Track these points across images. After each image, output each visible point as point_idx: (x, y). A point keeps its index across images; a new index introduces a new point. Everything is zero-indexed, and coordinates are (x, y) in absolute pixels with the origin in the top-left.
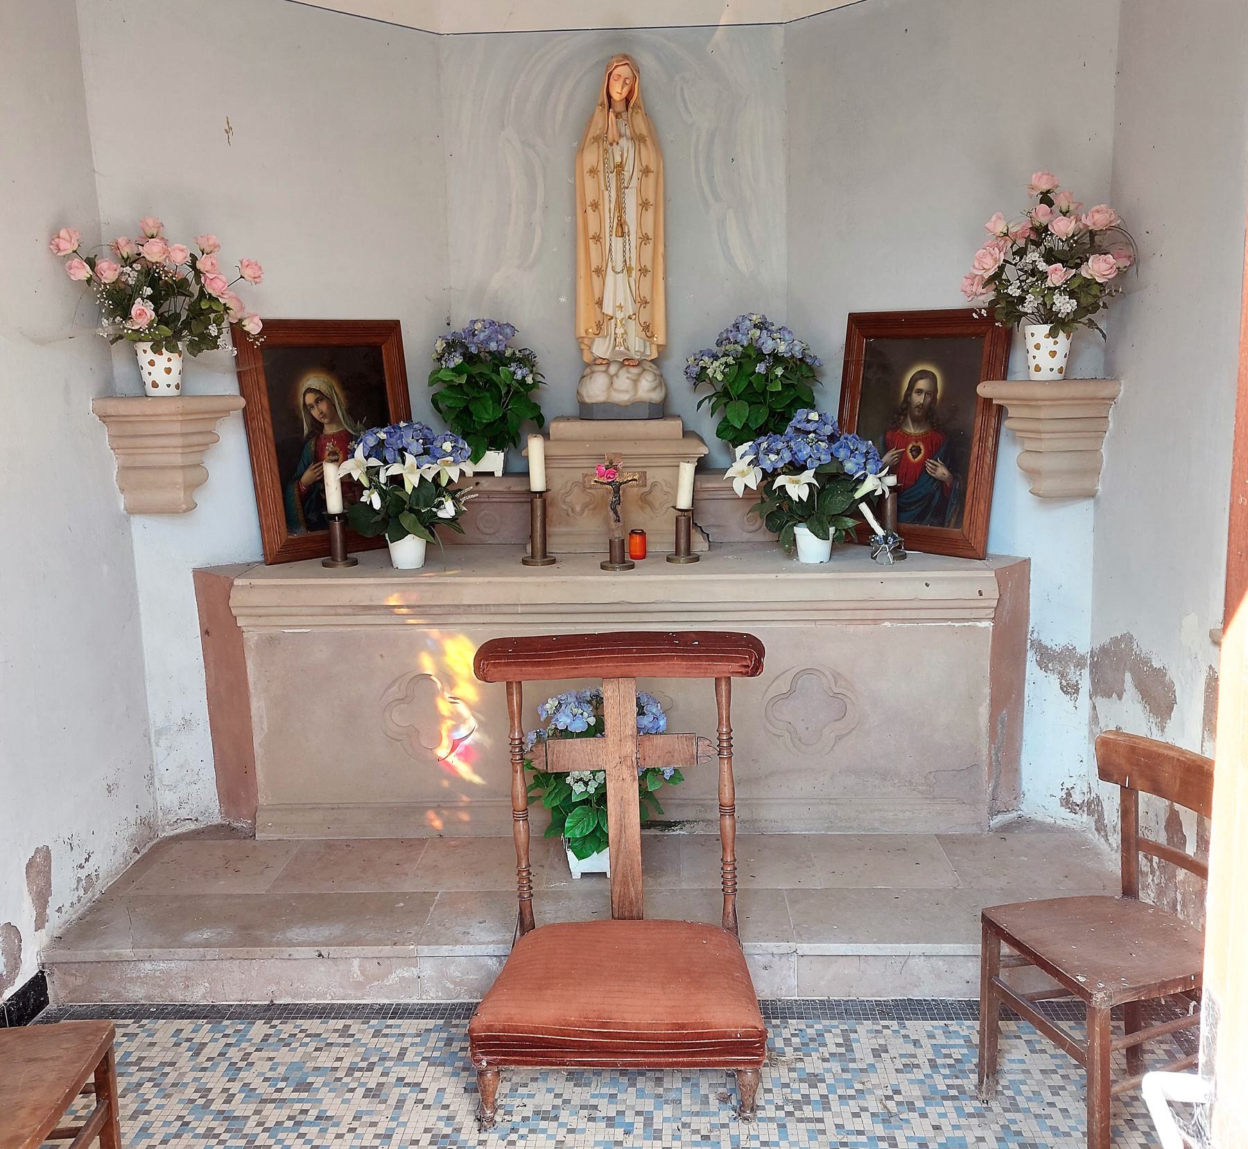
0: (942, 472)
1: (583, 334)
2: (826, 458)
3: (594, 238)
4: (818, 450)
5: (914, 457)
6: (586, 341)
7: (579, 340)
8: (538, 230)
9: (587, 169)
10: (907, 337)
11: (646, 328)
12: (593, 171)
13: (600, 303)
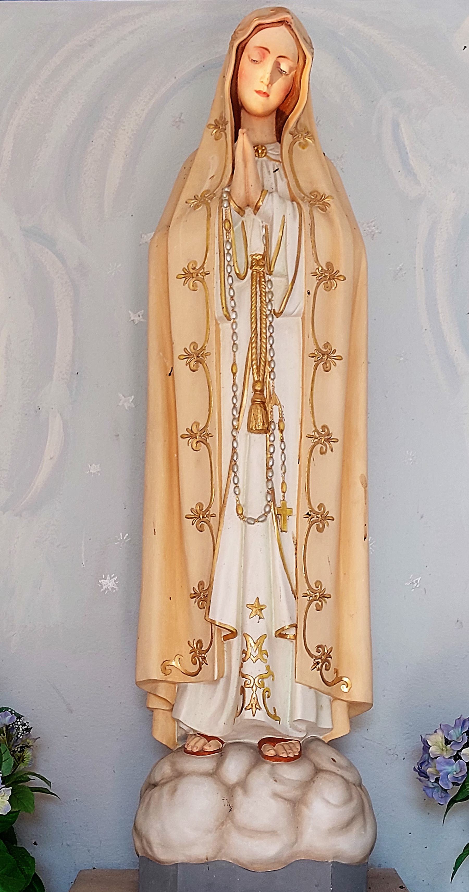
1: (156, 674)
3: (191, 435)
6: (162, 691)
7: (145, 689)
8: (56, 425)
9: (176, 267)
11: (323, 659)
12: (193, 275)
13: (203, 596)
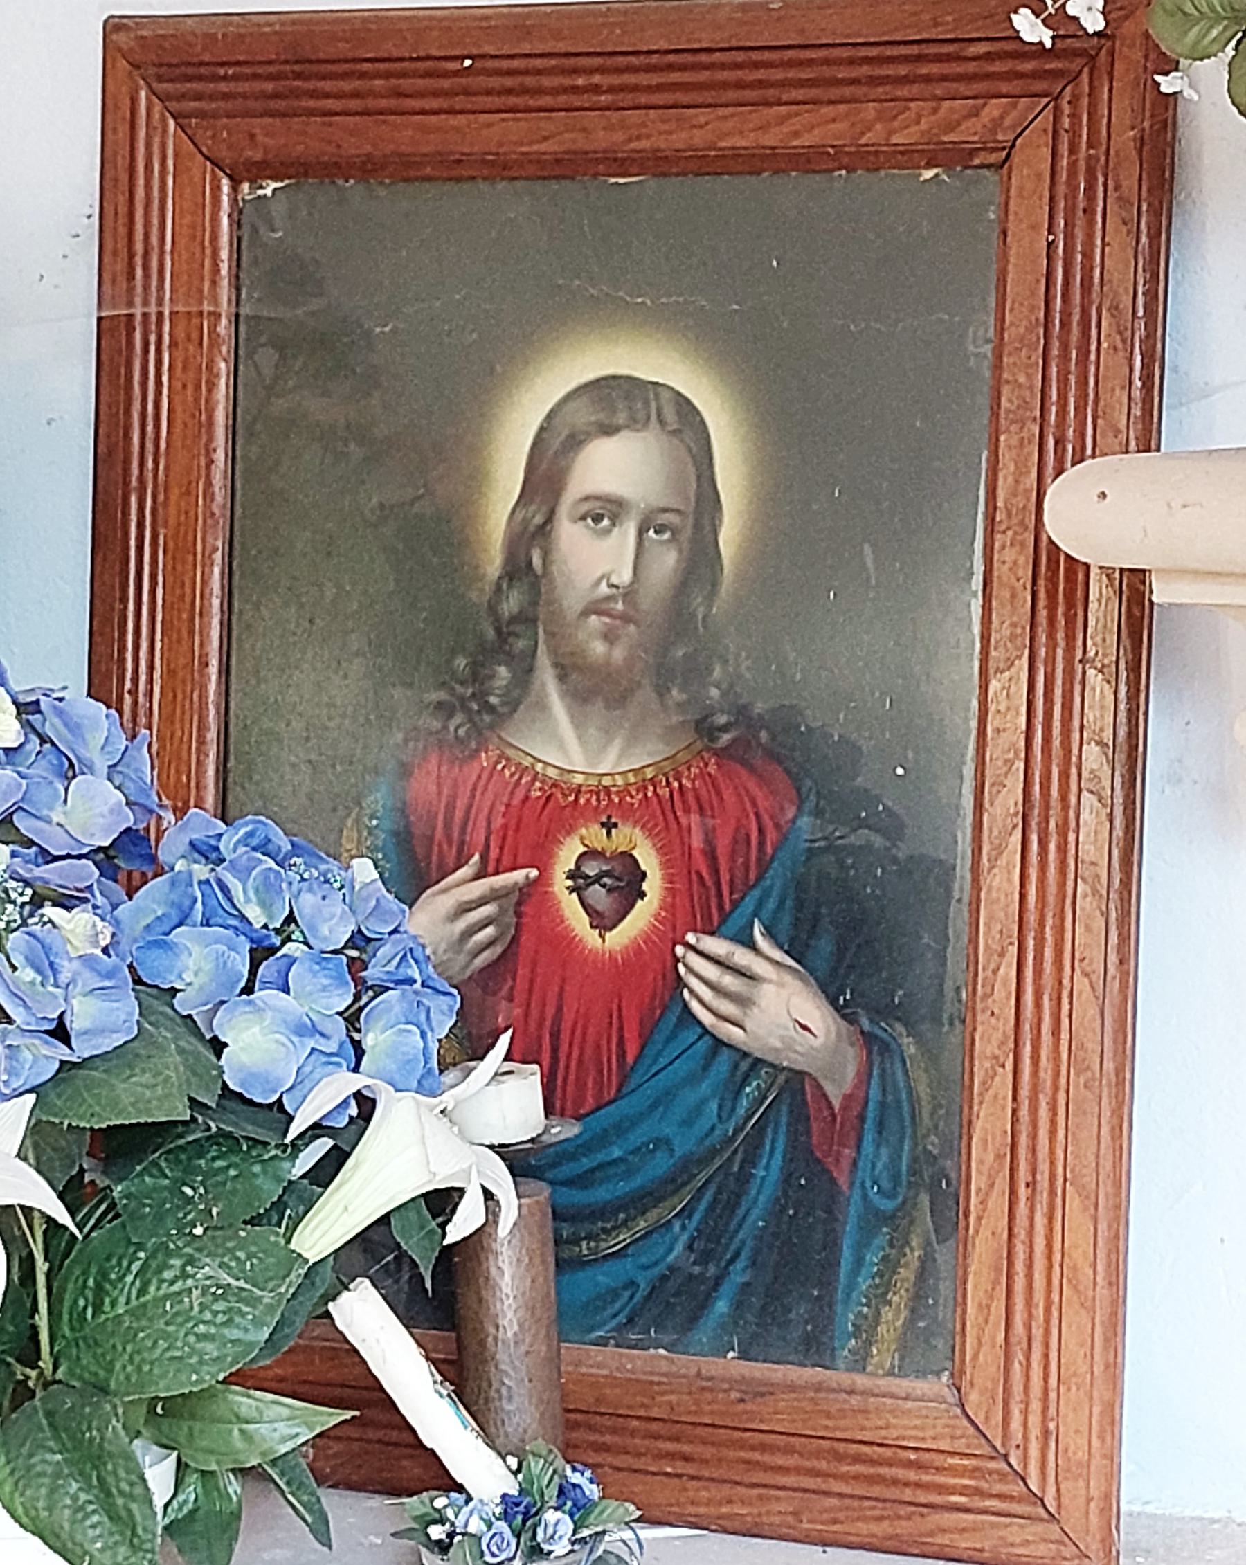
0: (780, 1011)
2: (104, 1019)
4: (46, 965)
5: (603, 923)
10: (499, 167)
